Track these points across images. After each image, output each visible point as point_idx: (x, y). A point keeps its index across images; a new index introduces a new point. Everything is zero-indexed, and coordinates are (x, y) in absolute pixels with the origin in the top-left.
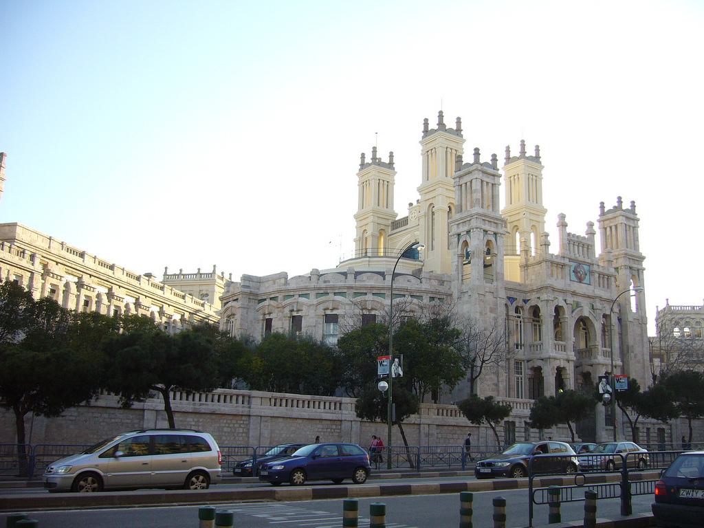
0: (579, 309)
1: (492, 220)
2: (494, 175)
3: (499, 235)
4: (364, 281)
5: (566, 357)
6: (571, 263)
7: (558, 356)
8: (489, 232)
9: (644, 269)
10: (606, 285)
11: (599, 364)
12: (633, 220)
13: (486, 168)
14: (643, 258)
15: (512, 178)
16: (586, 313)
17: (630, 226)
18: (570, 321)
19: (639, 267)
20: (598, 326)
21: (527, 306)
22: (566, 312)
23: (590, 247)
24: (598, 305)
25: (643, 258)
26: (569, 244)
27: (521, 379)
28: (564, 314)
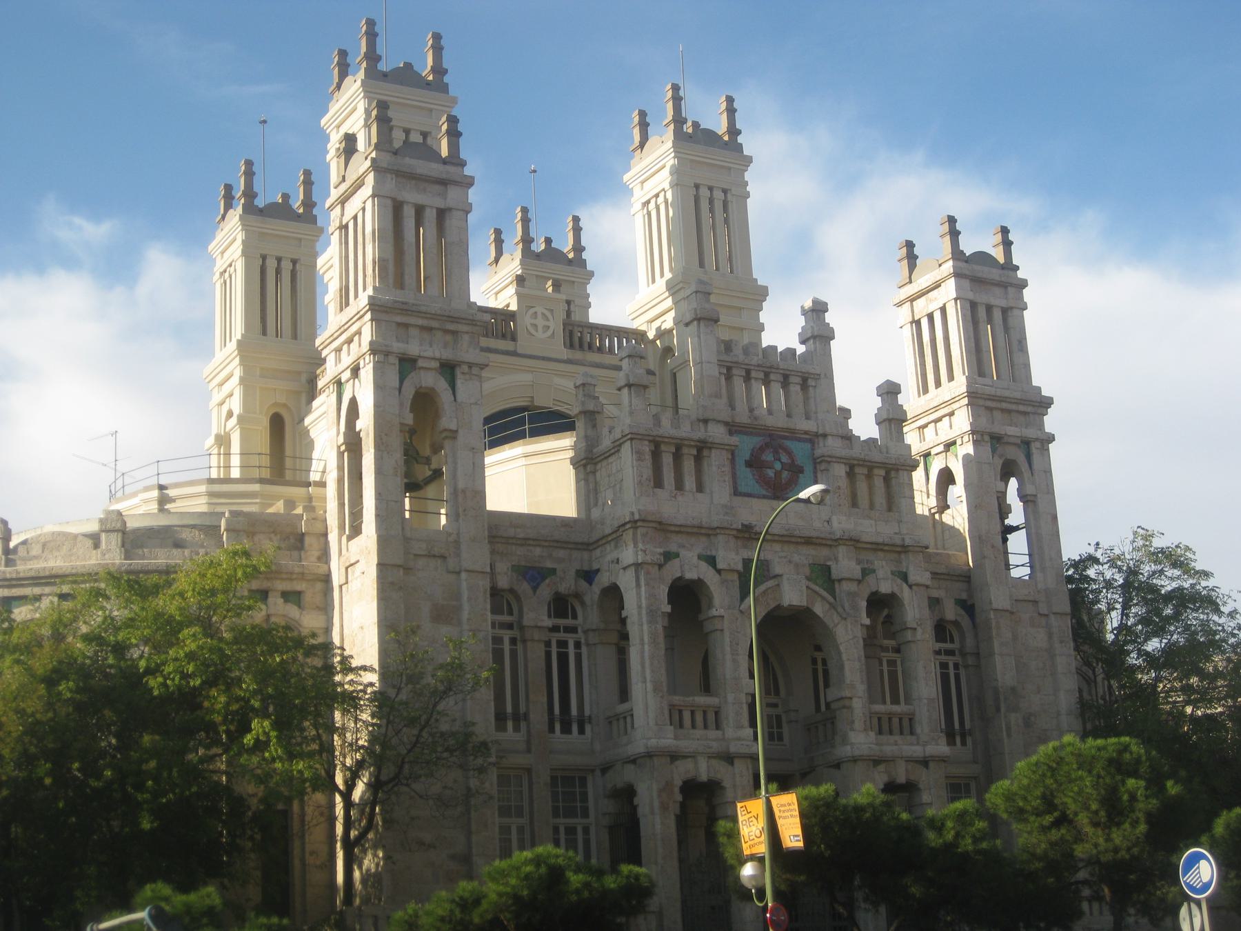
0: (770, 583)
1: (435, 324)
2: (444, 183)
3: (465, 368)
4: (35, 557)
5: (716, 746)
6: (735, 440)
7: (686, 745)
8: (421, 363)
9: (1051, 438)
10: (880, 499)
11: (855, 760)
12: (1004, 285)
13: (413, 162)
14: (1047, 403)
15: (652, 206)
16: (793, 595)
17: (989, 308)
18: (737, 631)
19: (1030, 433)
20: (848, 637)
21: (593, 593)
22: (717, 601)
23: (811, 382)
24: (845, 565)
25: (1047, 403)
26: (729, 377)
27: (586, 830)
28: (710, 606)
